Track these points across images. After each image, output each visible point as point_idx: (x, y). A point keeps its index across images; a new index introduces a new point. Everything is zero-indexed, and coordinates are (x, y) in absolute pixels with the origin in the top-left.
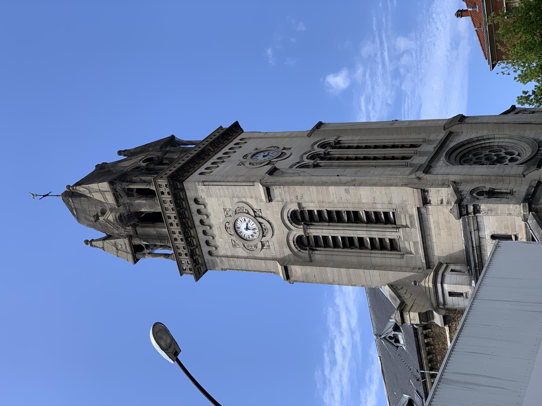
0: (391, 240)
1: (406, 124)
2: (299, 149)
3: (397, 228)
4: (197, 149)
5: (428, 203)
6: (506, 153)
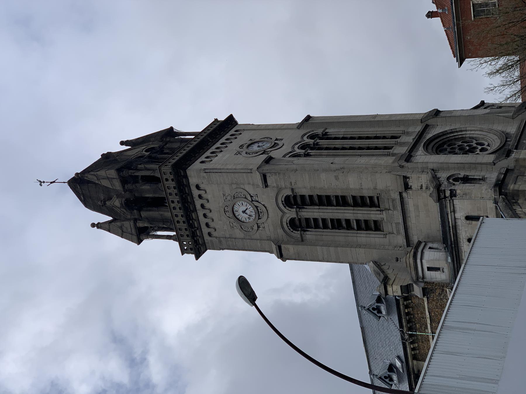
0: (375, 222)
1: (387, 117)
2: (297, 136)
3: (381, 211)
4: (196, 139)
5: (409, 188)
6: (477, 144)
